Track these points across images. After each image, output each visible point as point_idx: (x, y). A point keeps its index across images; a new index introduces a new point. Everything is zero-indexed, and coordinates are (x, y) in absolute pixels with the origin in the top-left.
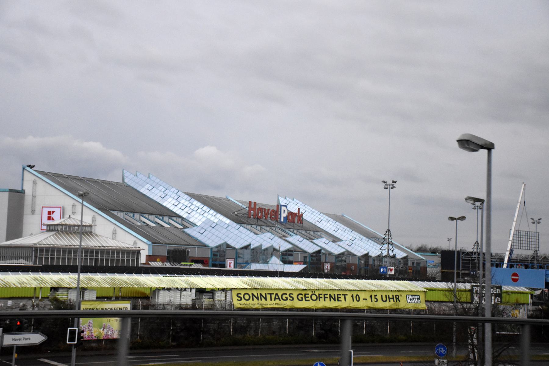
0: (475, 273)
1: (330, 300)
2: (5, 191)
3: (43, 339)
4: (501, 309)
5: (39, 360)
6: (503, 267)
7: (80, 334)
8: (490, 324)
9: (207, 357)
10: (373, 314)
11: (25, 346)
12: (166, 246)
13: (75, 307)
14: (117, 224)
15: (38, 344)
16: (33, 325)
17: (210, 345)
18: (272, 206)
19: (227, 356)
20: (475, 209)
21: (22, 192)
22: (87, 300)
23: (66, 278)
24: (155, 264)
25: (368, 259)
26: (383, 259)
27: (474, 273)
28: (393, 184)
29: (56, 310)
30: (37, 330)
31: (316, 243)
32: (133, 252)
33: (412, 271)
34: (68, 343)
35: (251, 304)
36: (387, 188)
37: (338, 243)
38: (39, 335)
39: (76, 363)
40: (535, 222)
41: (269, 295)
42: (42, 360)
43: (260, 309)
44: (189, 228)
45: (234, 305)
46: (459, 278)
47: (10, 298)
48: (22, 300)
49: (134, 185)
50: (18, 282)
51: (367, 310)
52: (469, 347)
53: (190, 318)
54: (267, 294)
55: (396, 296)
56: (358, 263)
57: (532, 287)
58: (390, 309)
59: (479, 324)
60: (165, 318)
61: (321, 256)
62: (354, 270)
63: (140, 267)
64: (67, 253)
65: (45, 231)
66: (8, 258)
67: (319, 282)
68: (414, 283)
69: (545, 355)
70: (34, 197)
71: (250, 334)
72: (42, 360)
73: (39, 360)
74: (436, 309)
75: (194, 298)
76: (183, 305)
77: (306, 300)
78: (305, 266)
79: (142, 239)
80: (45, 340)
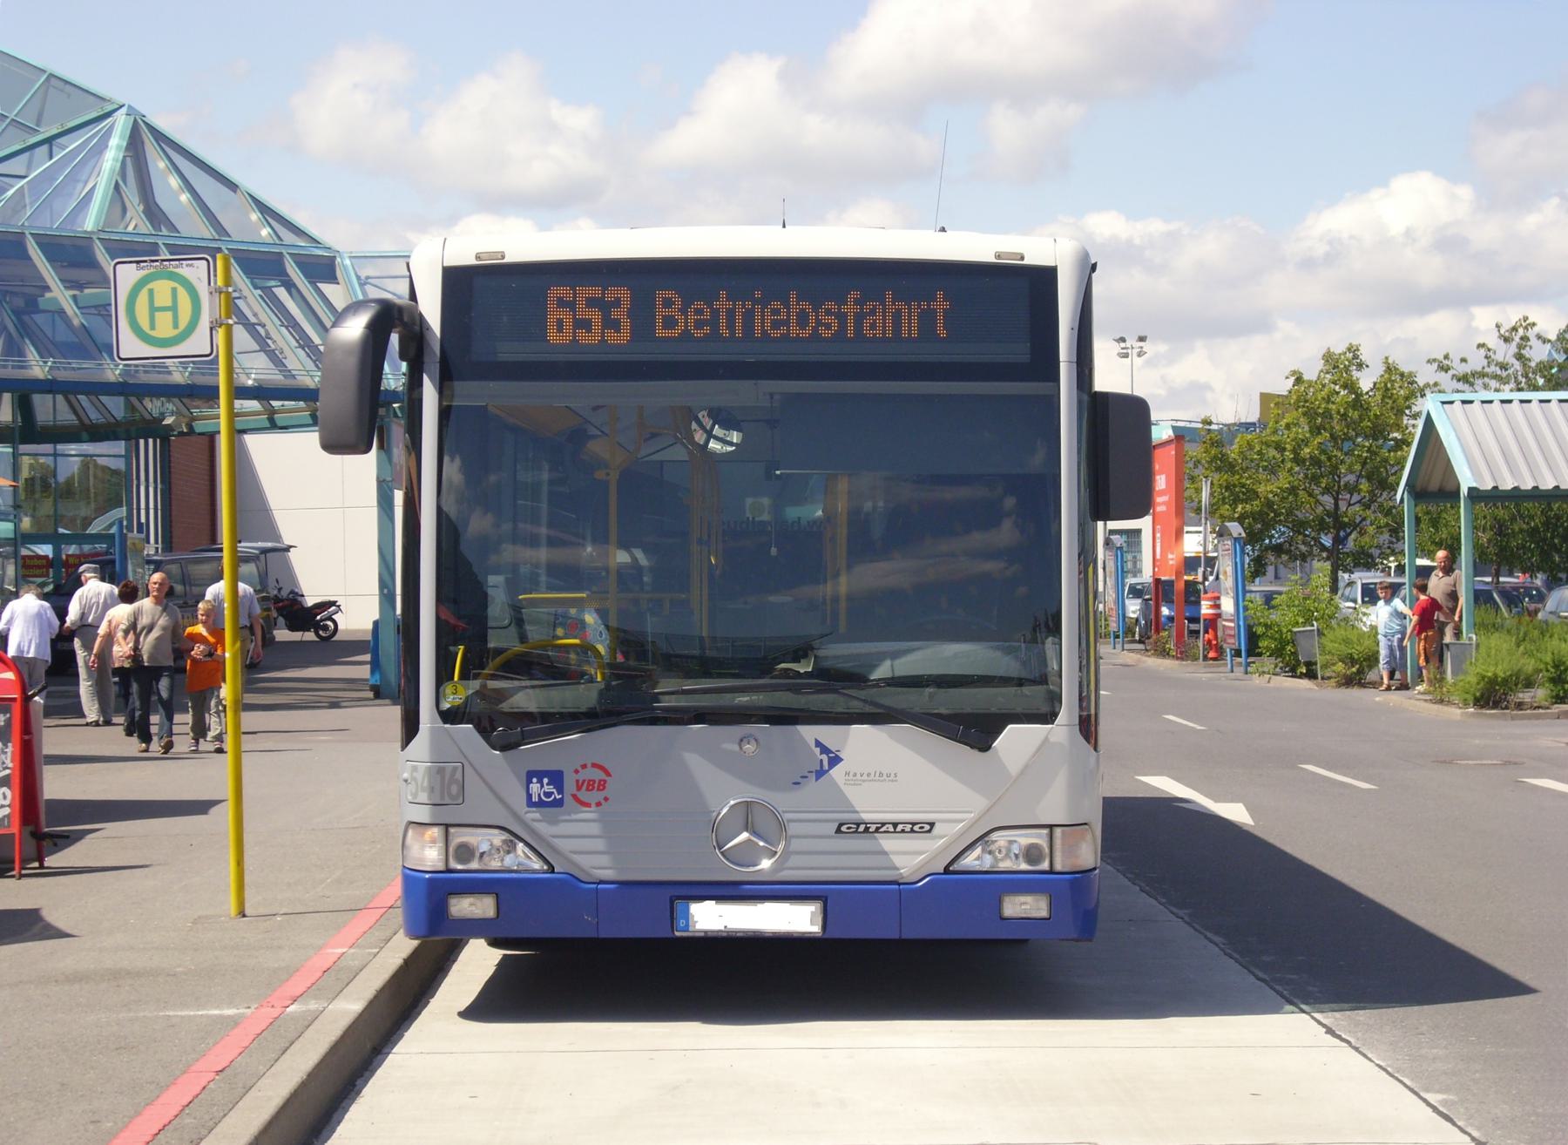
4: (1538, 575)
6: (237, 399)
20: (1126, 356)
21: (695, 716)
22: (496, 831)
23: (109, 494)
25: (1398, 369)
27: (1163, 503)
29: (218, 398)
35: (1536, 329)
38: (1167, 778)
40: (1129, 351)
42: (1167, 717)
47: (515, 466)
48: (806, 707)
54: (407, 260)
57: (288, 295)
58: (1197, 659)
60: (177, 1016)
61: (457, 281)
62: (381, 681)
66: (198, 368)
67: (29, 549)
68: (1202, 796)
69: (95, 138)
70: (394, 294)
71: (1187, 484)
72: (1167, 717)
75: (312, 438)
80: (817, 935)
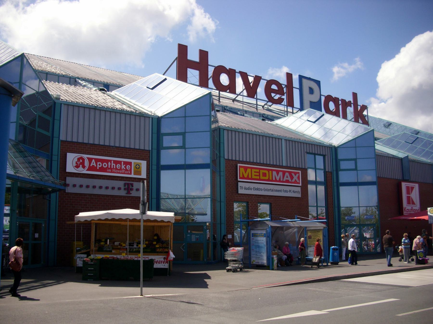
0: (215, 119)
1: (242, 187)
5: (397, 315)
6: (7, 179)
9: (394, 142)
10: (51, 140)
13: (168, 244)
16: (353, 104)
26: (315, 259)
31: (340, 264)
32: (21, 93)
37: (113, 93)
41: (66, 106)
44: (245, 173)
49: (221, 143)
50: (118, 86)
51: (306, 237)
52: (417, 240)
53: (60, 173)
59: (320, 264)
63: (302, 185)
64: (430, 157)
73: (397, 315)
74: (356, 250)
76: (216, 23)
79: (142, 109)
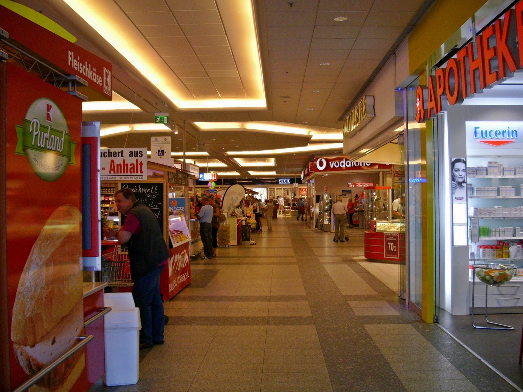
2: (510, 170)
3: (32, 150)
7: (97, 120)
8: (165, 326)
11: (107, 124)
12: (282, 189)
14: (166, 186)
15: (33, 248)
17: (167, 103)
18: (476, 95)
19: (48, 68)
24: (417, 181)
28: (479, 135)
30: (224, 160)
33: (162, 121)
34: (385, 257)
36: (433, 119)
39: (207, 169)
43: (105, 292)
45: (31, 357)
46: (129, 279)
55: (134, 172)
56: (210, 222)
58: (297, 178)
65: (431, 75)
77: (132, 152)
78: (511, 8)
